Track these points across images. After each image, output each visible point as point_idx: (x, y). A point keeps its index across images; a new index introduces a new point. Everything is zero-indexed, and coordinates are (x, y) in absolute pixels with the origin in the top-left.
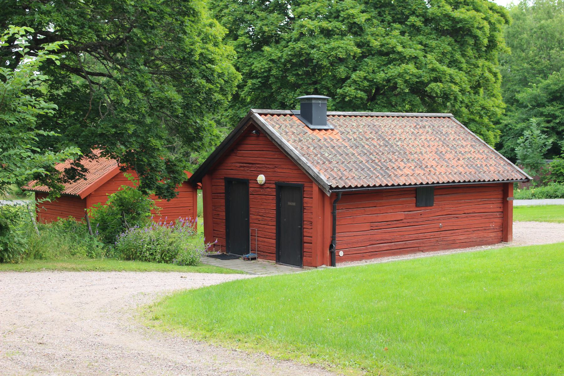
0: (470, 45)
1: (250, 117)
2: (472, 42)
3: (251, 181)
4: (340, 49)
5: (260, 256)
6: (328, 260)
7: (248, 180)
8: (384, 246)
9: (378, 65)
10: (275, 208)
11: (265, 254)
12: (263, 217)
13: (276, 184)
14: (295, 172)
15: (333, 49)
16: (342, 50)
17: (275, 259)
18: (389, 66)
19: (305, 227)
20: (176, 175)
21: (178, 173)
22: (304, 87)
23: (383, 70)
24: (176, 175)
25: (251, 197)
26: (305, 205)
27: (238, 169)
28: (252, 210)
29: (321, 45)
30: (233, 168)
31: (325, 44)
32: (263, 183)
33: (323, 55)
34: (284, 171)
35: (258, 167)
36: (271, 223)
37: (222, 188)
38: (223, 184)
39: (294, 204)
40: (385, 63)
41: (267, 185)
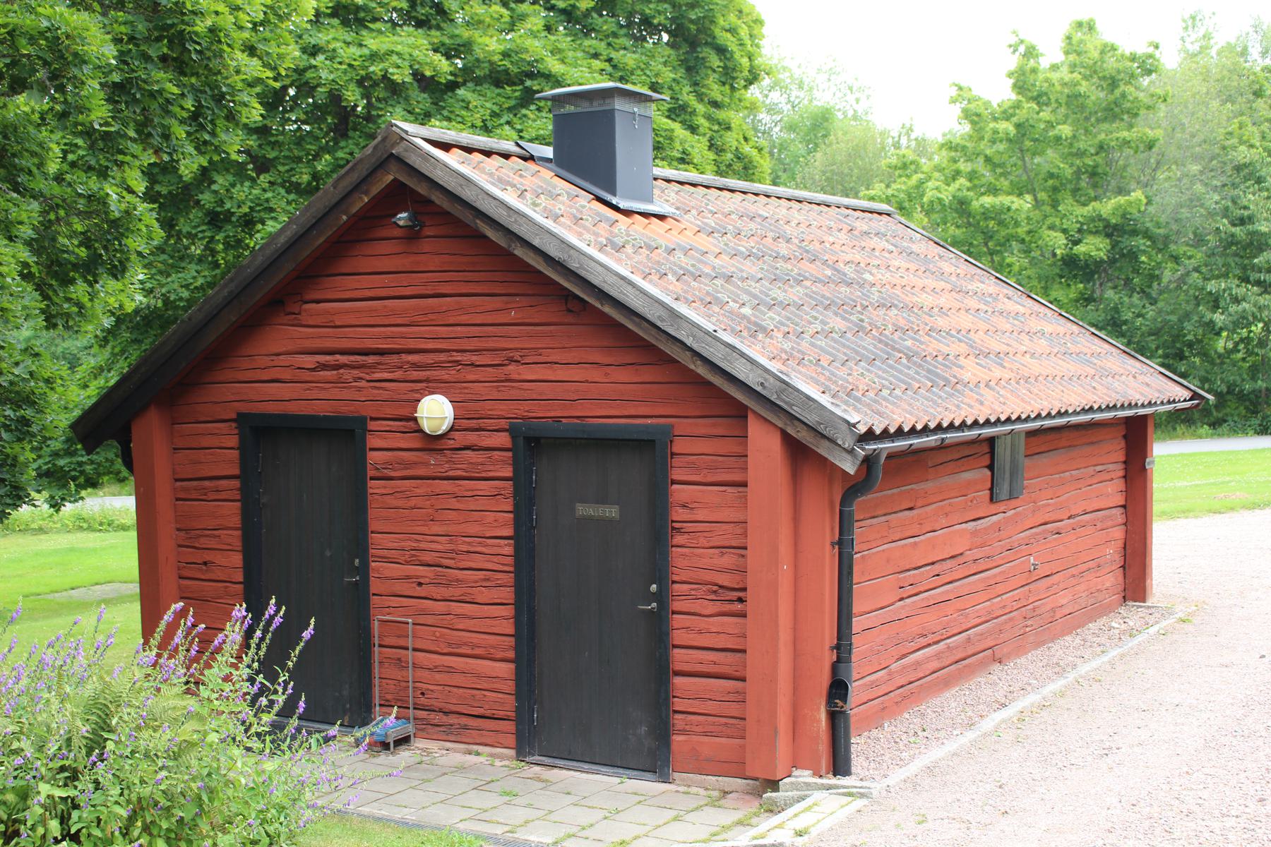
0: (714, 71)
1: (392, 156)
2: (715, 61)
3: (372, 425)
4: (395, 58)
5: (427, 728)
6: (823, 747)
7: (362, 421)
8: (928, 659)
9: (496, 109)
10: (508, 532)
11: (452, 719)
12: (442, 563)
13: (513, 431)
14: (648, 374)
15: (374, 57)
16: (399, 61)
17: (511, 740)
18: (524, 111)
19: (676, 605)
20: (28, 412)
21: (33, 404)
22: (281, 168)
23: (508, 123)
24: (28, 412)
25: (374, 487)
26: (678, 514)
27: (307, 376)
28: (379, 542)
29: (338, 45)
30: (285, 372)
31: (348, 44)
32: (445, 427)
33: (345, 72)
34: (561, 373)
35: (416, 366)
36: (484, 595)
37: (222, 452)
38: (233, 441)
39: (612, 512)
40: (512, 103)
41: (460, 438)
